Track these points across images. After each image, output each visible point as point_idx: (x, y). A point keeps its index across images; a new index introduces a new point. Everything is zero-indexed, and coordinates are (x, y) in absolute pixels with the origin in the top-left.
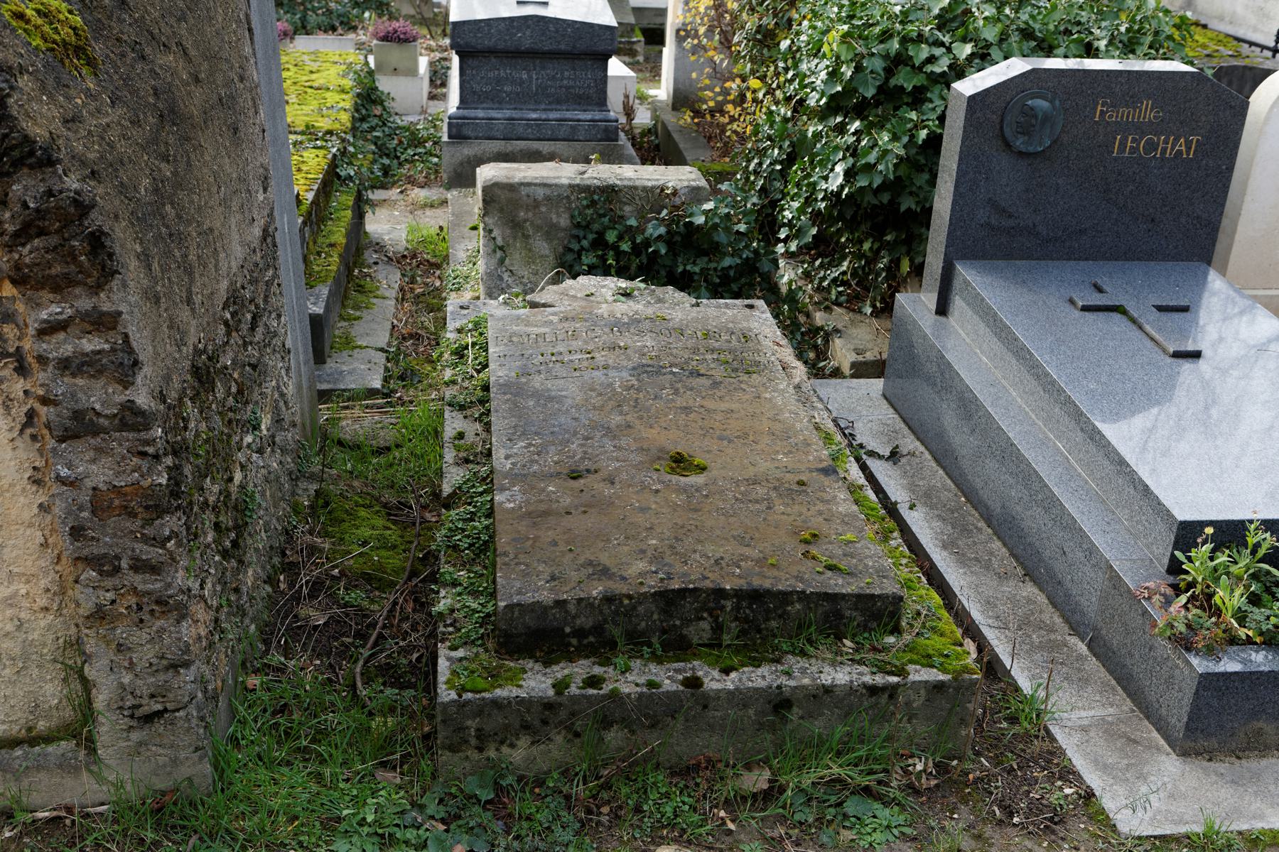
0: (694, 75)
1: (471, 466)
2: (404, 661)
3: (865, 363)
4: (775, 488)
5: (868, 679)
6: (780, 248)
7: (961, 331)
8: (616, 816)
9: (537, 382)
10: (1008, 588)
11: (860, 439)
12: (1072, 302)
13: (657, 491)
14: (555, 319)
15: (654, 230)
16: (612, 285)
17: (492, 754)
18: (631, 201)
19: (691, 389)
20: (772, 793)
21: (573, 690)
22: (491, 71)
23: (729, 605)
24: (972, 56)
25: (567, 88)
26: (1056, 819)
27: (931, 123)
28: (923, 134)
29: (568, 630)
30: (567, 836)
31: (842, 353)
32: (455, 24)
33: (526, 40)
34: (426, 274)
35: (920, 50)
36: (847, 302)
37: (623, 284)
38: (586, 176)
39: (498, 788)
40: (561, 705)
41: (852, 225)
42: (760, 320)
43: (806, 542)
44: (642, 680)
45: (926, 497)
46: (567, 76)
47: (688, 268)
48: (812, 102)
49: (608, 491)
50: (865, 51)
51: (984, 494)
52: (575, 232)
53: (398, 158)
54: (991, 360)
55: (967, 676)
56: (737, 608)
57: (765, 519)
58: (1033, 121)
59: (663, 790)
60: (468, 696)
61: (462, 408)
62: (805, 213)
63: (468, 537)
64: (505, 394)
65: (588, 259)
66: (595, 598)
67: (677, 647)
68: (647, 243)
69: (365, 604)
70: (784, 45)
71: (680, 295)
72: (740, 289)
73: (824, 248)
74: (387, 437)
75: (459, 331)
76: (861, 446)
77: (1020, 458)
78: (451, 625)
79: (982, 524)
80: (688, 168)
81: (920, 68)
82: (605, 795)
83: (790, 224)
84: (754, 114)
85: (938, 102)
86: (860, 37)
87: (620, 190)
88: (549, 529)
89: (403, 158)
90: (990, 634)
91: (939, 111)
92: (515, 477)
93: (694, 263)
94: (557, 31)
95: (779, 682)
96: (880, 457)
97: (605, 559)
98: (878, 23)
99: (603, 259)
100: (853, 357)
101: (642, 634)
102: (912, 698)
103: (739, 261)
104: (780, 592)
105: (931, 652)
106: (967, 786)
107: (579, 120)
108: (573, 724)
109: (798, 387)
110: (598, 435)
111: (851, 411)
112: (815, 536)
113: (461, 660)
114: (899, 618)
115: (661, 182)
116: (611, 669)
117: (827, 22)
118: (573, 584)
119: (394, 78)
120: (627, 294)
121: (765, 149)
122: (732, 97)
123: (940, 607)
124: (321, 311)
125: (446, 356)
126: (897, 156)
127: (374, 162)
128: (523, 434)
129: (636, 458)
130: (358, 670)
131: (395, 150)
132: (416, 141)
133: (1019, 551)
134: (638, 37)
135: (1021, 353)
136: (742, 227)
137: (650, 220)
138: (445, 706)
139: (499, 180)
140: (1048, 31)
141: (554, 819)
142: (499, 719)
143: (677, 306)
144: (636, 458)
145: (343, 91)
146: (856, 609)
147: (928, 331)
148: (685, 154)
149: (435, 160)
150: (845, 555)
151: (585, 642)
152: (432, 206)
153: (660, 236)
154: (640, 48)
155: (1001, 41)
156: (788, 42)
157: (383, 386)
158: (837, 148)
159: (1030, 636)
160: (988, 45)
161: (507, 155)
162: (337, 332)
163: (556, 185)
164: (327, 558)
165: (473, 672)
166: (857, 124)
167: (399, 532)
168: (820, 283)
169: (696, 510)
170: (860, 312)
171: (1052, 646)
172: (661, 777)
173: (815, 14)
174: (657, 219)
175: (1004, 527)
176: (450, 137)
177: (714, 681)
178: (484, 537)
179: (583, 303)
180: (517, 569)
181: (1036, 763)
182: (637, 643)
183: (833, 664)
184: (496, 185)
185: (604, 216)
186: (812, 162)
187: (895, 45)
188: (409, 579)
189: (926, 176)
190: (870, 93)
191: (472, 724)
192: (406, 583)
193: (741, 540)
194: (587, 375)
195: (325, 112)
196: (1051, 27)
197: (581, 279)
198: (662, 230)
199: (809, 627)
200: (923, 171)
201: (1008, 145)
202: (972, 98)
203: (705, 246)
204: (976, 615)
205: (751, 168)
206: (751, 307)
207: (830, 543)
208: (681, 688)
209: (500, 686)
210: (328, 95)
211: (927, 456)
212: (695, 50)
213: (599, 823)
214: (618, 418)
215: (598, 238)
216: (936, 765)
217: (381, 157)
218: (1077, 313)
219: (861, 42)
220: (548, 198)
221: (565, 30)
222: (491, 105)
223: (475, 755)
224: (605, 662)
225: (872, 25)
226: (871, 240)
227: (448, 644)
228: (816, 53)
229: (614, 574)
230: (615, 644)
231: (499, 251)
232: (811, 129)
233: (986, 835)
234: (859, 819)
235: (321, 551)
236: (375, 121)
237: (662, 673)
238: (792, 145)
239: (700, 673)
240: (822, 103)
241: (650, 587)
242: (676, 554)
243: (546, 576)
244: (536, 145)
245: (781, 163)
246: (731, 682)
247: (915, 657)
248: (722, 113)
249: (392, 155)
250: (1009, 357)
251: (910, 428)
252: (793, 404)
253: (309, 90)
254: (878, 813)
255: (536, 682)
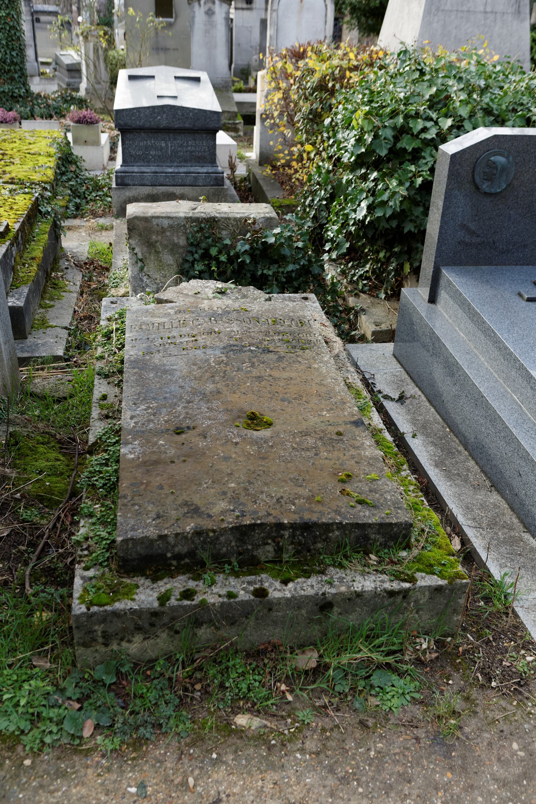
0: (271, 143)
1: (109, 421)
2: (61, 565)
3: (381, 332)
4: (321, 438)
5: (387, 586)
6: (326, 257)
7: (445, 315)
8: (206, 693)
9: (157, 359)
10: (480, 496)
11: (378, 387)
12: (520, 295)
13: (237, 443)
14: (172, 312)
15: (242, 247)
16: (213, 286)
17: (115, 647)
18: (226, 228)
19: (263, 363)
20: (321, 669)
21: (173, 602)
22: (142, 142)
23: (286, 534)
24: (451, 127)
25: (191, 152)
26: (522, 683)
27: (424, 173)
28: (419, 180)
29: (169, 555)
30: (168, 711)
31: (366, 326)
32: (118, 111)
33: (163, 121)
34: (100, 274)
35: (417, 123)
36: (369, 290)
37: (220, 285)
38: (196, 211)
39: (118, 673)
40: (163, 613)
41: (372, 241)
42: (309, 308)
43: (342, 481)
44: (223, 592)
45: (423, 428)
46: (192, 144)
47: (265, 272)
48: (345, 160)
49: (202, 444)
50: (380, 125)
51: (463, 428)
52: (190, 249)
53: (86, 198)
54: (466, 335)
55: (458, 581)
56: (293, 536)
57: (313, 464)
58: (495, 171)
59: (240, 671)
60: (95, 609)
61: (106, 376)
62: (342, 233)
63: (102, 478)
64: (134, 368)
65: (199, 267)
66: (188, 533)
67: (249, 565)
68: (237, 256)
69: (37, 519)
70: (327, 121)
71: (258, 292)
72: (299, 285)
73: (354, 255)
74: (65, 389)
75: (109, 320)
76: (380, 392)
77: (487, 407)
78: (86, 549)
79: (461, 448)
80: (264, 205)
81: (417, 136)
82: (198, 675)
83: (332, 240)
84: (308, 167)
85: (429, 159)
86: (377, 115)
87: (219, 220)
88: (157, 475)
89: (89, 198)
90: (470, 533)
91: (430, 165)
92: (137, 434)
93: (269, 269)
94: (183, 115)
95: (323, 590)
96: (392, 400)
97: (197, 500)
98: (389, 105)
99: (209, 266)
100: (373, 328)
101: (224, 556)
102: (419, 597)
103: (298, 267)
104: (324, 524)
105: (433, 562)
106: (458, 657)
107: (199, 173)
108: (173, 625)
109: (337, 356)
110: (197, 399)
111: (372, 366)
112: (349, 476)
113: (91, 579)
114: (410, 538)
115: (246, 215)
116: (201, 583)
117: (355, 105)
118: (172, 522)
119: (85, 147)
120: (222, 292)
121: (316, 191)
122: (295, 157)
123: (438, 525)
124: (22, 304)
125: (99, 337)
126: (402, 196)
127: (70, 201)
128: (145, 399)
129: (222, 417)
130: (28, 573)
131: (84, 193)
132: (98, 187)
133: (487, 469)
134: (240, 120)
135: (488, 332)
136: (300, 244)
137: (239, 240)
138: (78, 617)
139: (138, 215)
140: (501, 109)
141: (160, 697)
142: (118, 625)
143: (255, 301)
144: (222, 417)
145: (50, 156)
146: (379, 533)
147: (423, 315)
148: (267, 193)
149: (109, 199)
150: (371, 491)
151: (183, 562)
152: (106, 229)
153: (246, 251)
154: (241, 127)
155: (470, 117)
156: (329, 120)
157: (65, 354)
158: (362, 191)
159: (496, 533)
160: (462, 120)
161: (153, 195)
162: (37, 317)
163: (176, 218)
164: (13, 485)
165: (99, 589)
166: (375, 174)
167: (66, 462)
168: (352, 278)
169: (264, 458)
170: (377, 297)
171: (513, 541)
172: (238, 661)
173: (347, 100)
174: (244, 240)
175: (476, 451)
176: (117, 185)
177: (277, 591)
178: (114, 479)
179: (192, 300)
180: (132, 509)
181: (506, 635)
182: (220, 561)
183: (363, 574)
184: (136, 218)
185: (208, 238)
186: (345, 200)
187: (400, 120)
188: (70, 498)
189: (421, 209)
190: (383, 153)
191: (99, 629)
192: (67, 502)
193: (296, 482)
194: (192, 353)
195: (37, 169)
196: (504, 107)
197: (193, 282)
198: (247, 247)
199: (345, 548)
200: (419, 205)
201: (477, 188)
202: (454, 156)
203: (276, 257)
204: (461, 519)
205: (307, 203)
206: (306, 299)
207: (360, 481)
208: (252, 597)
209: (119, 600)
210: (40, 158)
211: (423, 398)
212: (274, 126)
213: (192, 698)
214: (212, 386)
215: (206, 254)
216: (437, 642)
217: (75, 198)
218: (524, 303)
219: (378, 118)
220: (171, 227)
221: (188, 114)
222: (142, 164)
223: (103, 649)
224: (197, 578)
225: (385, 107)
226: (384, 251)
227: (83, 565)
228: (348, 126)
229: (203, 512)
230: (205, 564)
231: (140, 262)
232: (345, 178)
233: (473, 697)
234: (382, 688)
235: (9, 479)
236: (70, 175)
237: (238, 585)
238: (333, 188)
239: (266, 585)
240: (352, 160)
241: (229, 523)
242: (249, 495)
243: (153, 515)
244: (171, 189)
245: (326, 199)
246: (288, 591)
247: (421, 567)
248: (290, 167)
249: (82, 196)
250: (479, 334)
251: (411, 378)
252: (334, 372)
253: (28, 155)
254: (395, 683)
255: (146, 596)
